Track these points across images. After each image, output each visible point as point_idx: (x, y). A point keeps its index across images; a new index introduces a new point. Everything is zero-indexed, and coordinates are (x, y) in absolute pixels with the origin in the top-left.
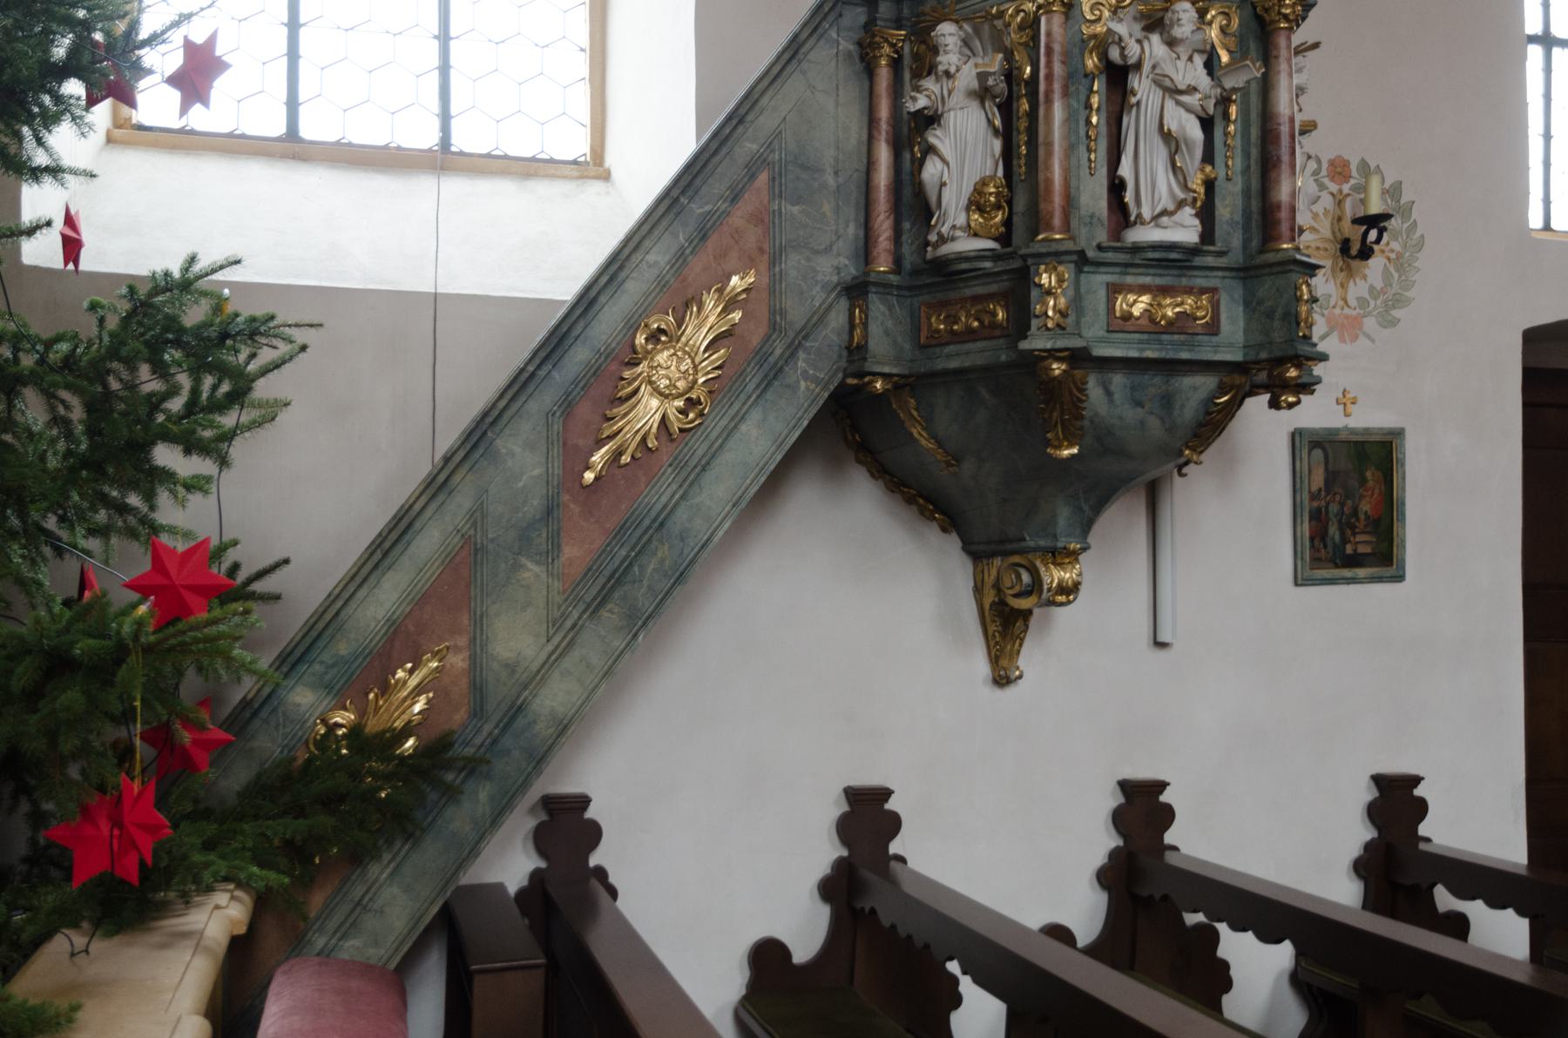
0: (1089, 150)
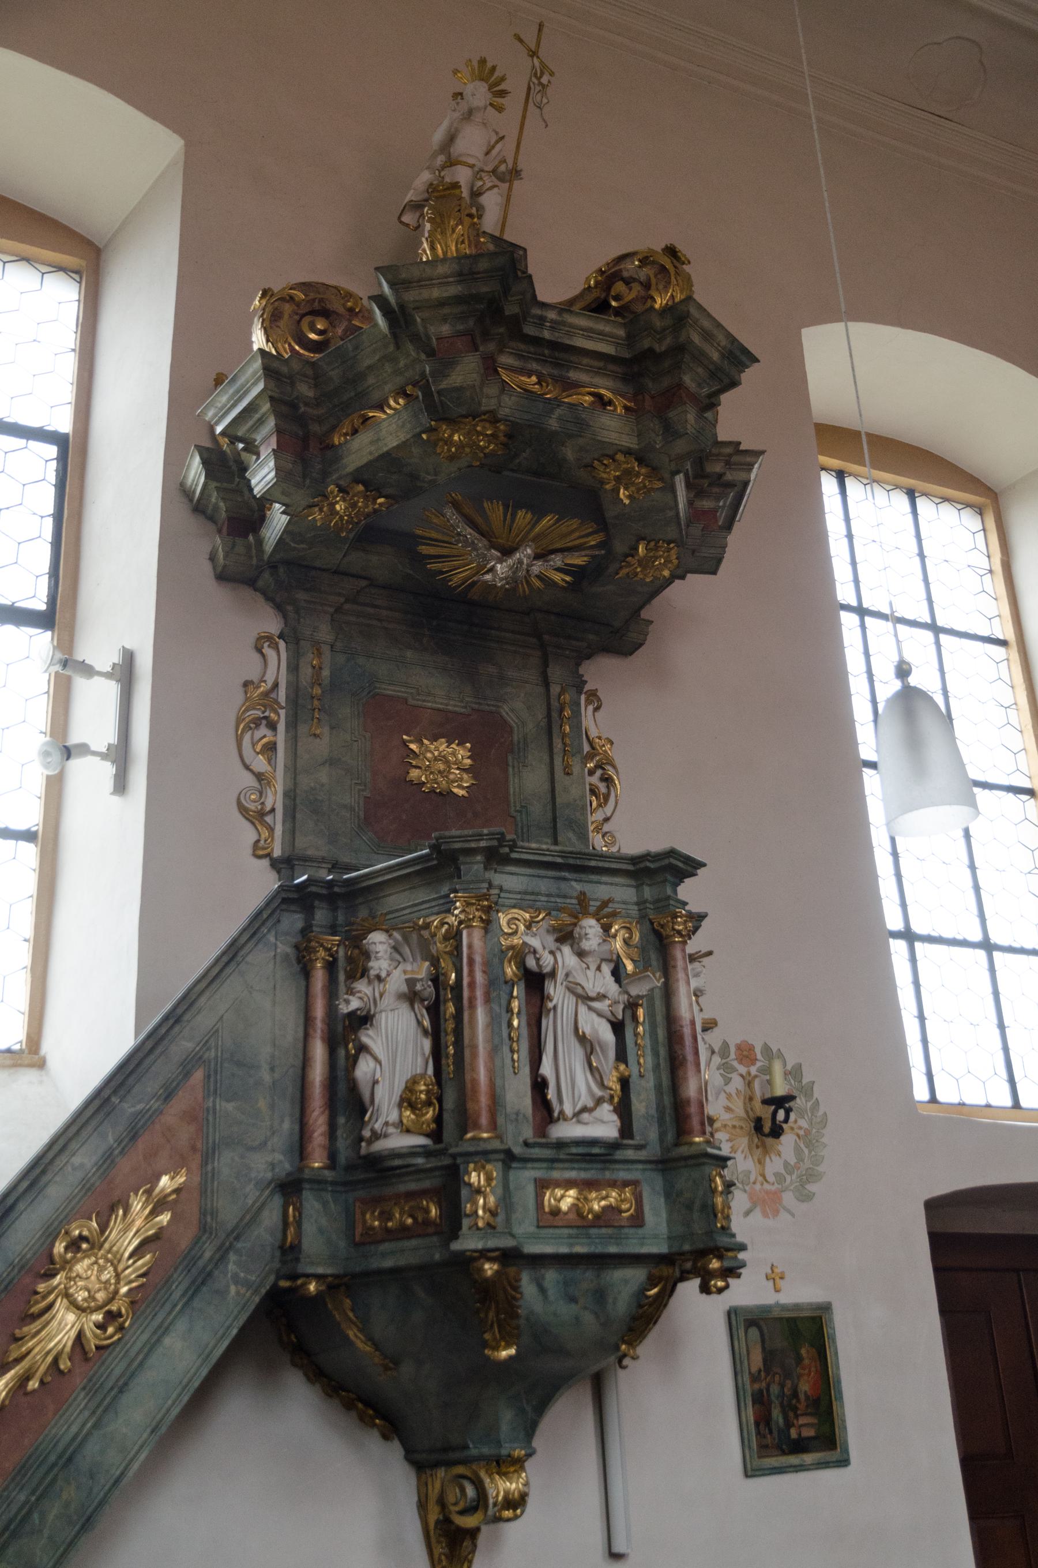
0: (512, 1051)
